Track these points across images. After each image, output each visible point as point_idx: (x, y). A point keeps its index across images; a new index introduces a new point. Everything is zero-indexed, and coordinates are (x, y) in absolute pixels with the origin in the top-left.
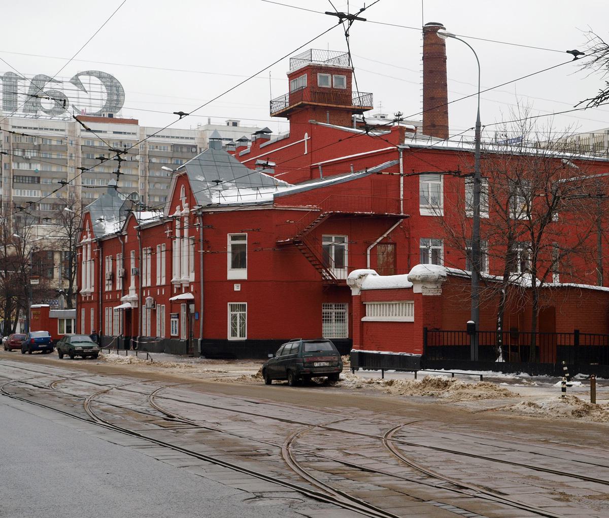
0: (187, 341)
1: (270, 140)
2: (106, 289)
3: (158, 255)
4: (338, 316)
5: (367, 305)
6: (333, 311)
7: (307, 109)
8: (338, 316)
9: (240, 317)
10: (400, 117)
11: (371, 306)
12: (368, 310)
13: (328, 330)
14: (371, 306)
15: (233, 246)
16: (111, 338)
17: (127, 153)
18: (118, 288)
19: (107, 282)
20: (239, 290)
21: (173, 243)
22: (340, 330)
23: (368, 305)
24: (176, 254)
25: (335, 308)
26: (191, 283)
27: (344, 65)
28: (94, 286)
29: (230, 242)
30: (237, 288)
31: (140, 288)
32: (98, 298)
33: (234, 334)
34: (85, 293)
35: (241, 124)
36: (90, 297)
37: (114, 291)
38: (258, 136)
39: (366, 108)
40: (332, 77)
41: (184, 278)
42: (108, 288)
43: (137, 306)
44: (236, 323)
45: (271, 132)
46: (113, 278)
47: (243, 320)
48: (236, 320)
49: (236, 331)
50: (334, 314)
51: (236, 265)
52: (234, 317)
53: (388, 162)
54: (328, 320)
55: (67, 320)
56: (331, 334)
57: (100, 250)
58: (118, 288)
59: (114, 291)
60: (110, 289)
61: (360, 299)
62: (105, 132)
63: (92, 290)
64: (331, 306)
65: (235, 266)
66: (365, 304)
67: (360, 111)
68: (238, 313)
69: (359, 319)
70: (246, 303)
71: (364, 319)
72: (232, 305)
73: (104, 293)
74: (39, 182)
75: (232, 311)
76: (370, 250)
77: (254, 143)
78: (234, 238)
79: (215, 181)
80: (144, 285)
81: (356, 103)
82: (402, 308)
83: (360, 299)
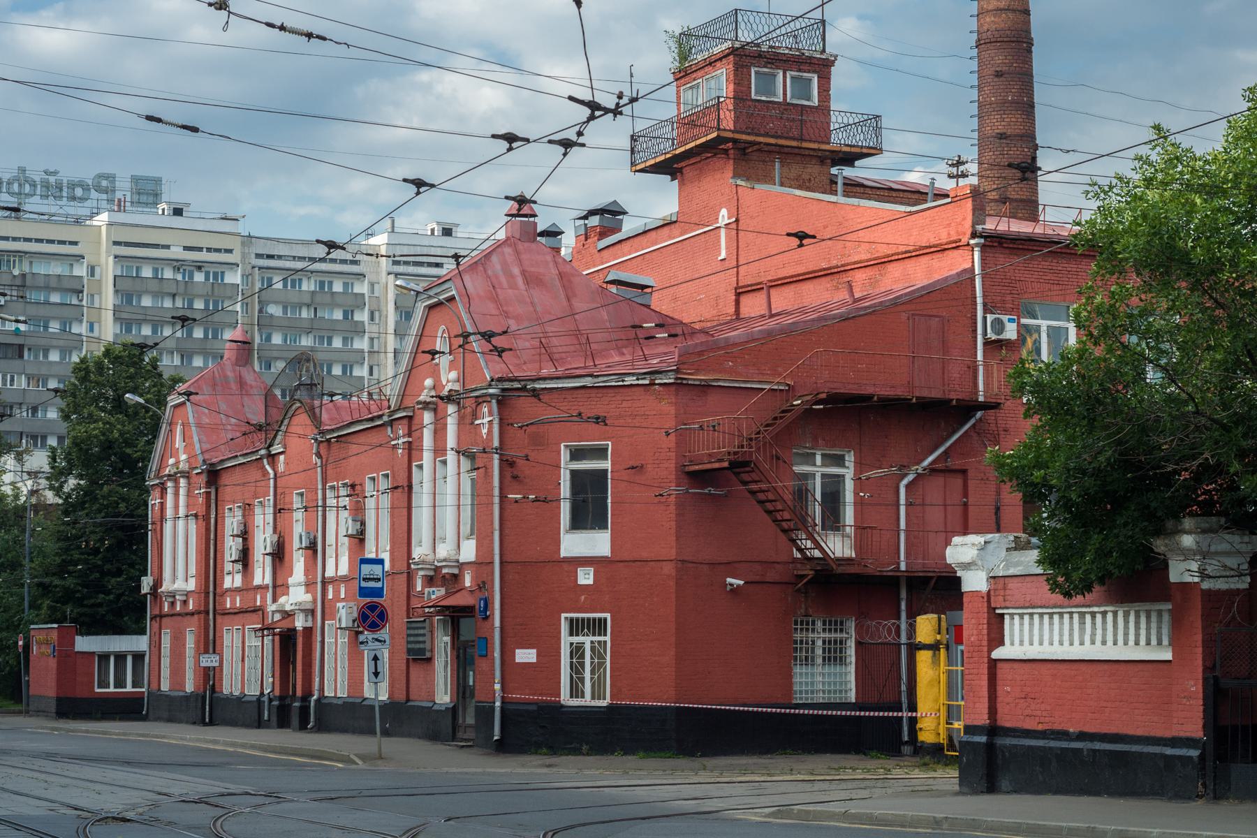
0: (454, 710)
1: (620, 230)
2: (227, 583)
3: (370, 503)
4: (835, 652)
5: (1007, 617)
6: (819, 636)
7: (726, 151)
8: (835, 652)
9: (593, 649)
10: (961, 168)
11: (1051, 618)
12: (1012, 630)
13: (807, 683)
14: (1051, 618)
15: (575, 474)
16: (240, 701)
17: (621, 113)
18: (257, 581)
19: (228, 567)
20: (590, 582)
21: (414, 469)
22: (835, 683)
23: (1012, 615)
24: (422, 498)
25: (824, 630)
26: (462, 566)
27: (808, 46)
28: (197, 576)
29: (567, 467)
30: (586, 577)
31: (319, 579)
32: (207, 603)
33: (576, 691)
34: (172, 595)
35: (459, 233)
36: (185, 602)
37: (248, 589)
38: (594, 221)
39: (865, 151)
40: (785, 77)
41: (179, 585)
42: (232, 580)
43: (309, 624)
44: (582, 665)
45: (625, 213)
46: (245, 558)
47: (601, 657)
48: (582, 656)
49: (583, 684)
50: (819, 643)
51: (588, 513)
52: (577, 651)
53: (449, 420)
54: (806, 658)
55: (100, 656)
56: (812, 692)
57: (213, 491)
58: (257, 581)
59: (248, 589)
60: (238, 581)
61: (989, 601)
62: (168, 247)
63: (192, 585)
64: (813, 623)
65: (578, 523)
66: (1002, 615)
67: (849, 159)
68: (587, 640)
69: (986, 654)
70: (608, 616)
71: (997, 654)
72: (571, 620)
73: (219, 593)
74: (21, 356)
75: (571, 635)
76: (907, 486)
77: (583, 238)
78: (576, 455)
79: (795, 235)
80: (330, 573)
81: (838, 139)
82: (1126, 622)
83: (989, 601)
